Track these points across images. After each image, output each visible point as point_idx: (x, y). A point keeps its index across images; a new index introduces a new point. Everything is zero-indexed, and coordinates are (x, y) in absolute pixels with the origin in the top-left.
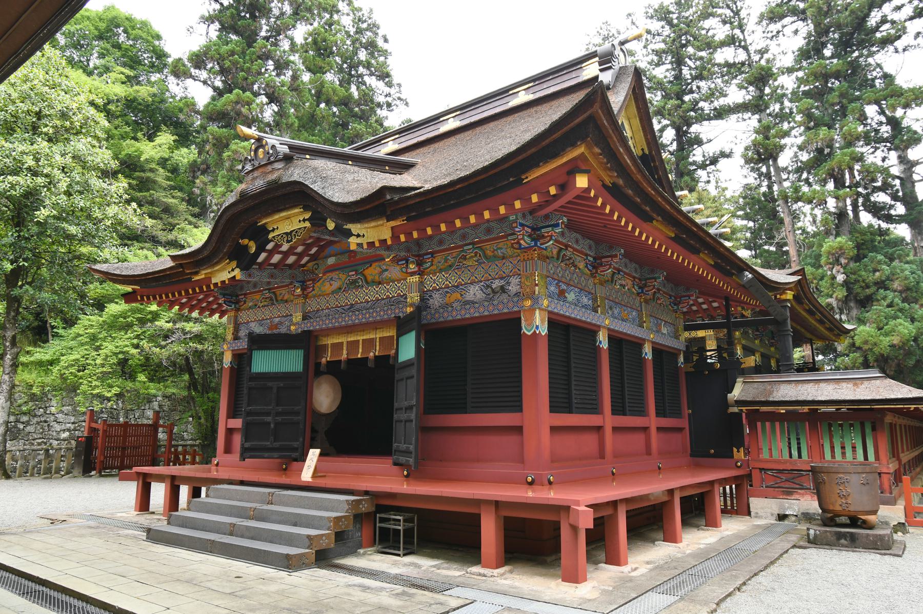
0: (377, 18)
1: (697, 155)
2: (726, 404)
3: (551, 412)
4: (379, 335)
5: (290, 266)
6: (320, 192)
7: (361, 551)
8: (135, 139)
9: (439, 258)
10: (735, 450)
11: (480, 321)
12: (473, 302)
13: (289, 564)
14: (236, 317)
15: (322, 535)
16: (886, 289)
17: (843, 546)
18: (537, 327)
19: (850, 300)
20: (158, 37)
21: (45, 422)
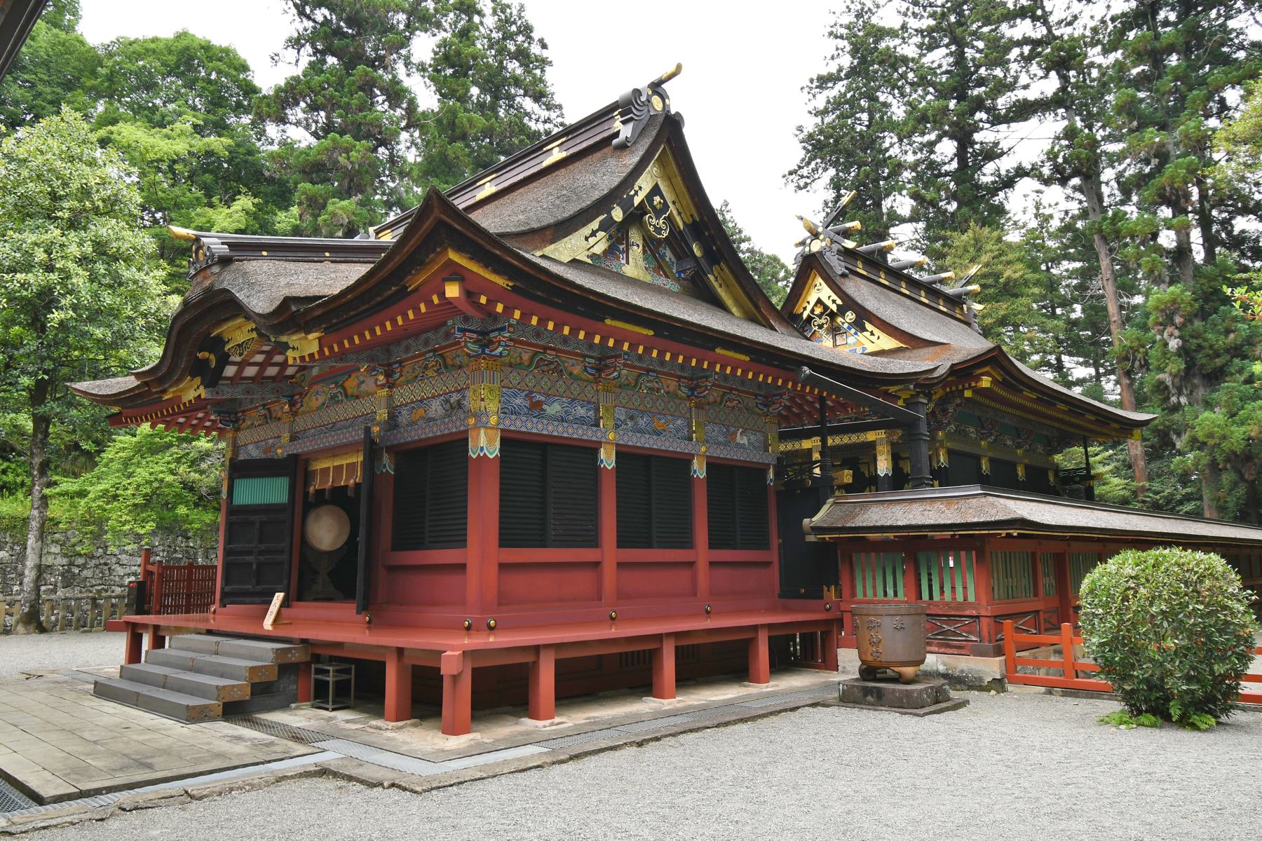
0: (530, 17)
1: (987, 175)
2: (802, 533)
3: (500, 546)
4: (344, 461)
5: (273, 378)
6: (245, 301)
7: (293, 705)
8: (211, 205)
9: (408, 367)
10: (825, 588)
12: (434, 419)
13: (195, 716)
14: (234, 440)
15: (234, 686)
16: (1244, 357)
17: (870, 704)
18: (482, 449)
19: (1194, 375)
20: (244, 68)
21: (106, 564)
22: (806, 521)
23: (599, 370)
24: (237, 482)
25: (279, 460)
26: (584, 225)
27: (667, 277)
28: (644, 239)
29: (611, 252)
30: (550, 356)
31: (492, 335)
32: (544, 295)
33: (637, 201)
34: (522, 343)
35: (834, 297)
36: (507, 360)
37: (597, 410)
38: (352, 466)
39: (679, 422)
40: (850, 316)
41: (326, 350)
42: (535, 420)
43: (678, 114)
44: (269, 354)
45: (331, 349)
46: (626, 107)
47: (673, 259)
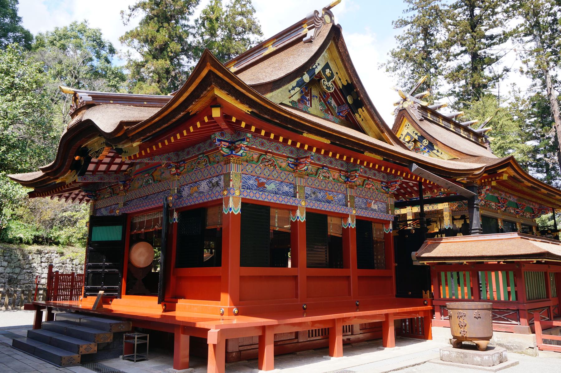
3: (242, 265)
5: (115, 172)
10: (424, 292)
11: (250, 202)
12: (202, 192)
22: (413, 254)
23: (296, 165)
24: (94, 229)
25: (117, 217)
26: (289, 82)
27: (332, 115)
28: (320, 94)
29: (302, 100)
30: (269, 156)
31: (237, 143)
32: (269, 118)
33: (317, 71)
34: (253, 149)
35: (416, 132)
36: (245, 158)
37: (295, 188)
38: (156, 220)
39: (340, 196)
40: (425, 142)
41: (143, 152)
42: (261, 193)
43: (338, 25)
44: (113, 158)
45: (146, 151)
46: (312, 21)
47: (336, 105)
